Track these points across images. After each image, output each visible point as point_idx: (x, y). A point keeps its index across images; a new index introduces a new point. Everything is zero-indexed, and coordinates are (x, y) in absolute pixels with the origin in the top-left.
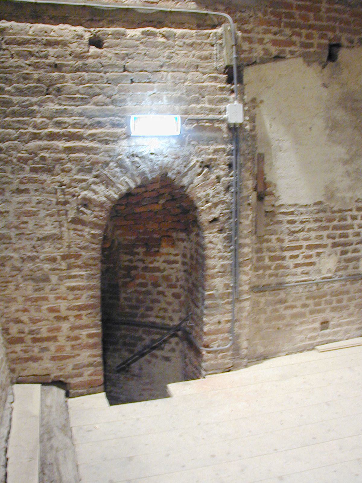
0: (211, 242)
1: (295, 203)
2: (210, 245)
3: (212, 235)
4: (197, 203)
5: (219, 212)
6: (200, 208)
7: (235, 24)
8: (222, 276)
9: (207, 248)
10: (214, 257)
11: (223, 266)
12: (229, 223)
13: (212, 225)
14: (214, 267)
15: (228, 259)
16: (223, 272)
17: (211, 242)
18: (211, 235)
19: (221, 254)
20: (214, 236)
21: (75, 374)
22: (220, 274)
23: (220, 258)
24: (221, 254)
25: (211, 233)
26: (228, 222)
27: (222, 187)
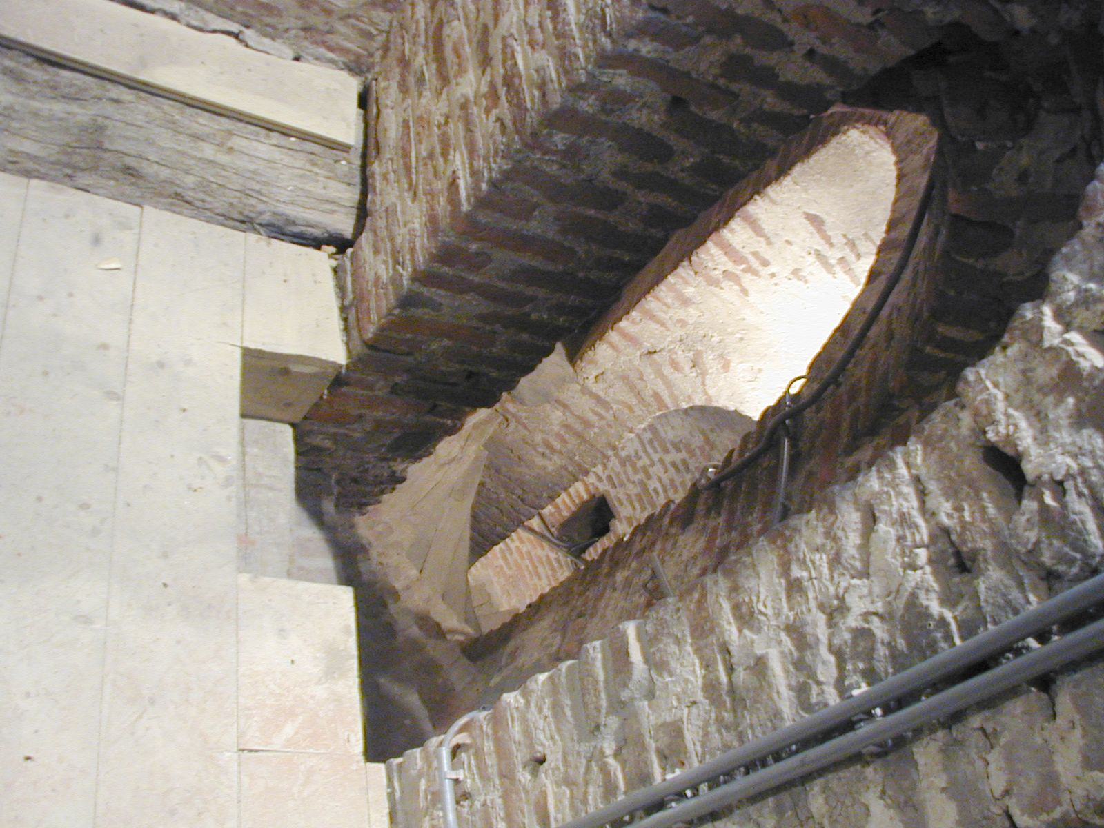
0: (871, 518)
1: (329, 181)
2: (851, 517)
3: (911, 504)
4: (1068, 260)
5: (1063, 463)
6: (1047, 310)
7: (1085, 223)
8: (711, 687)
9: (832, 510)
10: (795, 588)
11: (760, 666)
12: (1015, 594)
13: (972, 463)
14: (746, 617)
15: (801, 691)
16: (732, 690)
17: (871, 518)
18: (909, 490)
19: (819, 628)
20: (904, 520)
21: (772, 683)
22: (724, 678)
23: (796, 631)
24: (819, 628)
25: (922, 494)
26: (1020, 585)
27: (672, 436)
